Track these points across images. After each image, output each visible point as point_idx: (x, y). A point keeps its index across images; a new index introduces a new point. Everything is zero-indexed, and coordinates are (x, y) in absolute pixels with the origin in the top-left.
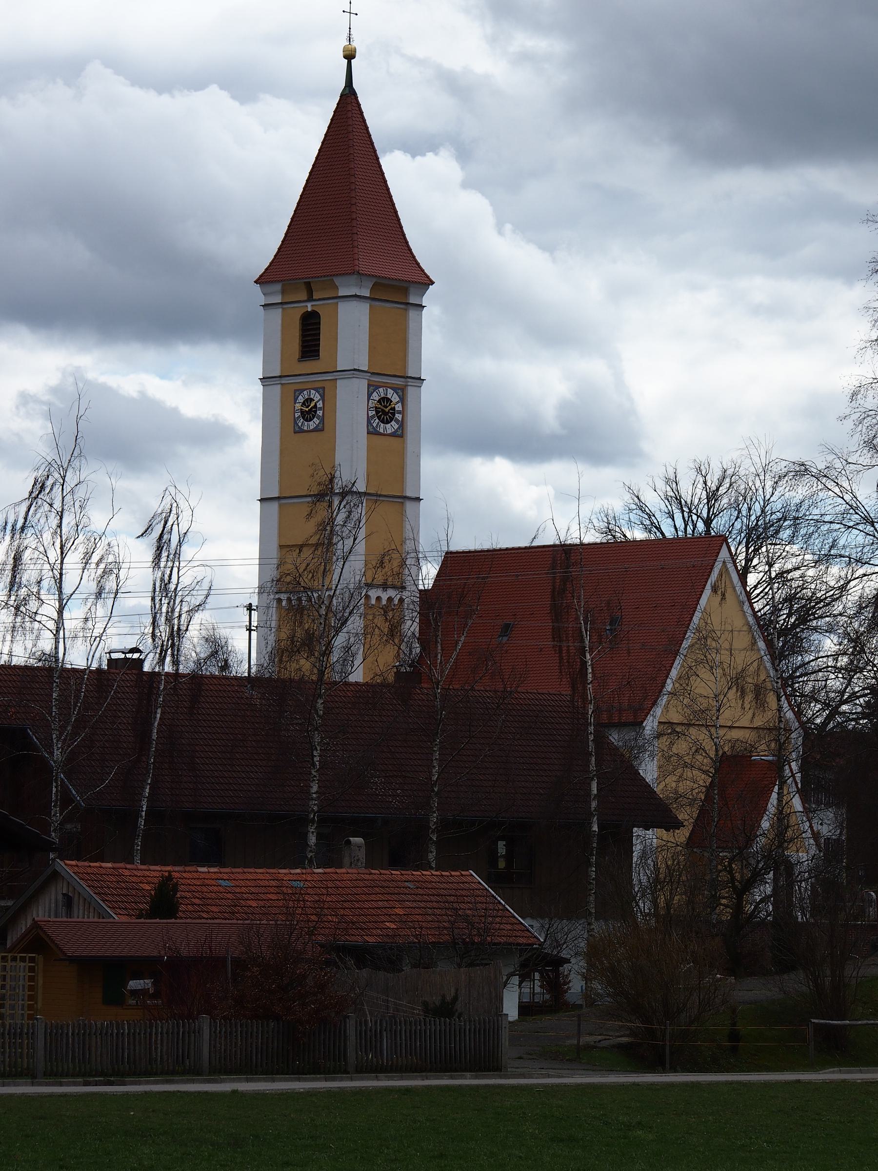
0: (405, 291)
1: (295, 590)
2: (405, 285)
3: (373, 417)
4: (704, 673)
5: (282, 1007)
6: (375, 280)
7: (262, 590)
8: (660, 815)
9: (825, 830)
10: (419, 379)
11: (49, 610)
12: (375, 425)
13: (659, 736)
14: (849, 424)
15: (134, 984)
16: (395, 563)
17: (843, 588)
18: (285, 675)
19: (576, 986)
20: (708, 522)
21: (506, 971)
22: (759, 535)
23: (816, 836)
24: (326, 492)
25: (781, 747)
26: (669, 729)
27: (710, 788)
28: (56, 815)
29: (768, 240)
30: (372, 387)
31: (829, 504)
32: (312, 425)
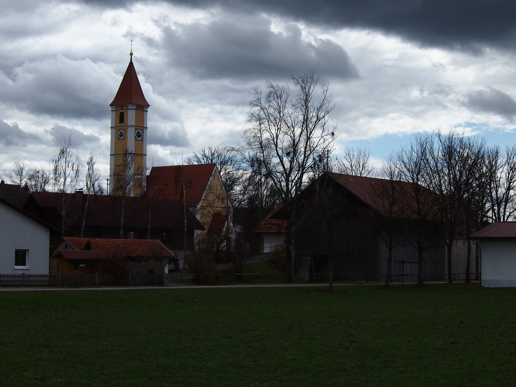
0: (144, 108)
1: (118, 175)
4: (210, 195)
5: (114, 271)
7: (110, 176)
8: (200, 227)
9: (238, 230)
11: (62, 180)
13: (200, 209)
14: (244, 139)
15: (81, 265)
16: (141, 170)
17: (242, 176)
18: (115, 195)
19: (181, 266)
20: (212, 161)
21: (165, 263)
22: (224, 163)
23: (236, 232)
24: (126, 154)
25: (228, 211)
26: (203, 207)
27: (212, 221)
28: (64, 227)
29: (219, 97)
30: (136, 129)
31: (239, 157)
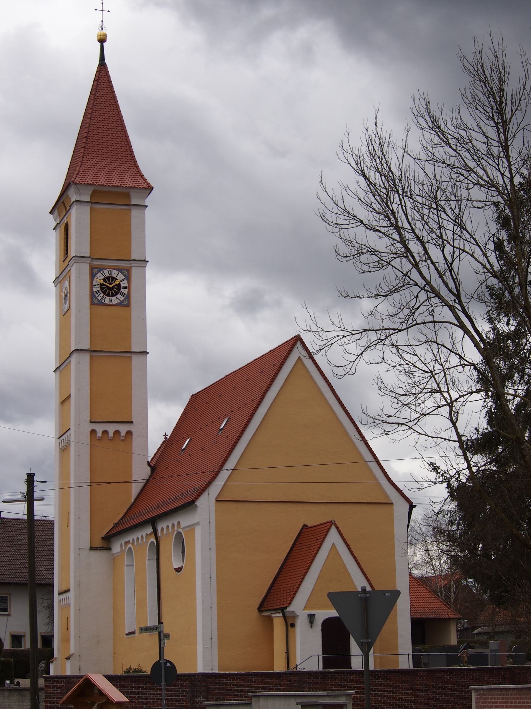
2: (125, 190)
3: (97, 292)
6: (93, 188)
10: (144, 261)
12: (99, 298)
32: (115, 300)
